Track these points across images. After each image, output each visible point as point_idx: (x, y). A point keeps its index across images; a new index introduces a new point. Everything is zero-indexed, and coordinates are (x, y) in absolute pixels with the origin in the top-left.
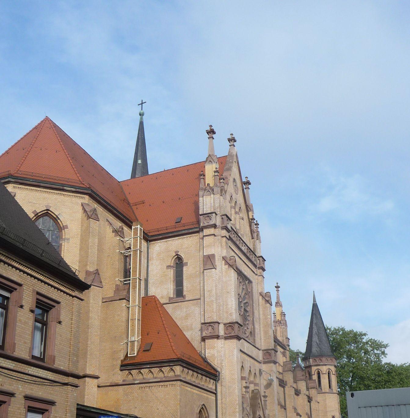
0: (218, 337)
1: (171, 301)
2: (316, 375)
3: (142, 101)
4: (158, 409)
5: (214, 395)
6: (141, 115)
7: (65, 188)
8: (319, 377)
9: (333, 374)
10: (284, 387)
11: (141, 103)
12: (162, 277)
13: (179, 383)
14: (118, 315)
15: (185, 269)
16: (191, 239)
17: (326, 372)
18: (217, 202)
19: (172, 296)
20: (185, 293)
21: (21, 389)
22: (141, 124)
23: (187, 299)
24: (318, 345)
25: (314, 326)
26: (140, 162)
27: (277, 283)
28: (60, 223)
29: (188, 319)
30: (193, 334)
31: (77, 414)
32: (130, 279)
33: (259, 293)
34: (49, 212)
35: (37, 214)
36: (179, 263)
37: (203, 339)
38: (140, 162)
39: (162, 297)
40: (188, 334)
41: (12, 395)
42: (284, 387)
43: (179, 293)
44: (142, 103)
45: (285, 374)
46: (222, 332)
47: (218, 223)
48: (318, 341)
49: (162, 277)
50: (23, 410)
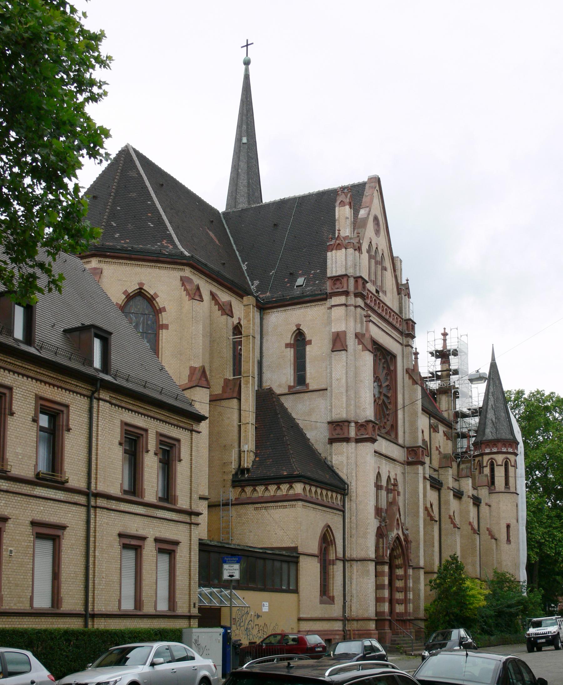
0: (347, 440)
1: (292, 392)
2: (489, 466)
3: (247, 41)
4: (276, 534)
5: (341, 513)
6: (247, 63)
7: (161, 259)
8: (492, 470)
9: (512, 466)
10: (439, 490)
11: (246, 44)
12: (279, 358)
13: (300, 503)
14: (229, 418)
15: (308, 348)
16: (316, 309)
17: (502, 463)
18: (350, 258)
19: (292, 384)
20: (308, 381)
21: (152, 532)
22: (247, 78)
23: (311, 388)
24: (494, 424)
25: (490, 396)
26: (245, 140)
27: (445, 329)
28: (156, 305)
29: (311, 416)
30: (317, 435)
31: (200, 550)
32: (241, 378)
33: (405, 371)
34: (143, 291)
35: (129, 294)
36: (300, 340)
37: (332, 441)
38: (245, 140)
39: (280, 386)
40: (310, 435)
41: (143, 539)
42: (439, 490)
43: (300, 377)
44: (247, 45)
45: (441, 471)
46: (352, 433)
47: (352, 288)
48: (494, 419)
49: (279, 358)
50: (154, 552)
